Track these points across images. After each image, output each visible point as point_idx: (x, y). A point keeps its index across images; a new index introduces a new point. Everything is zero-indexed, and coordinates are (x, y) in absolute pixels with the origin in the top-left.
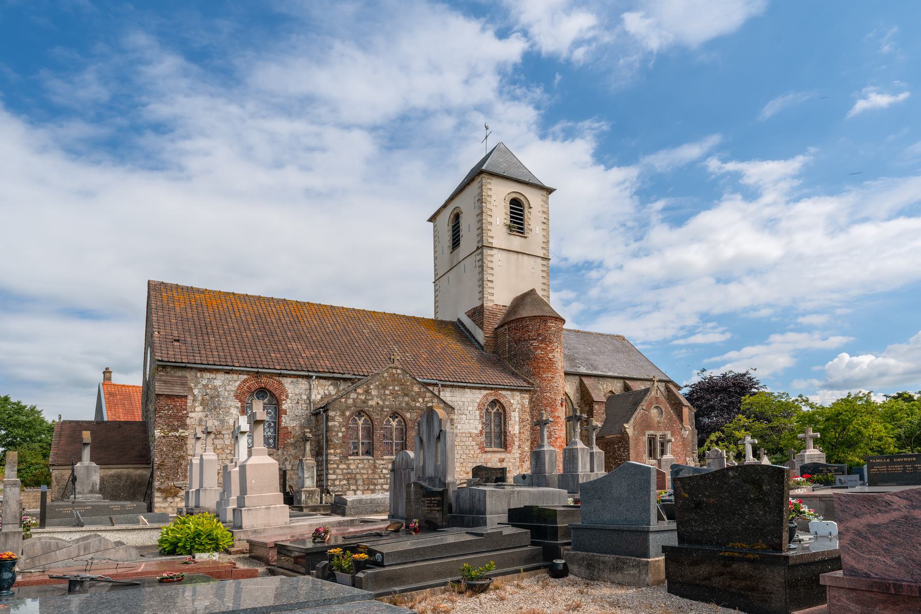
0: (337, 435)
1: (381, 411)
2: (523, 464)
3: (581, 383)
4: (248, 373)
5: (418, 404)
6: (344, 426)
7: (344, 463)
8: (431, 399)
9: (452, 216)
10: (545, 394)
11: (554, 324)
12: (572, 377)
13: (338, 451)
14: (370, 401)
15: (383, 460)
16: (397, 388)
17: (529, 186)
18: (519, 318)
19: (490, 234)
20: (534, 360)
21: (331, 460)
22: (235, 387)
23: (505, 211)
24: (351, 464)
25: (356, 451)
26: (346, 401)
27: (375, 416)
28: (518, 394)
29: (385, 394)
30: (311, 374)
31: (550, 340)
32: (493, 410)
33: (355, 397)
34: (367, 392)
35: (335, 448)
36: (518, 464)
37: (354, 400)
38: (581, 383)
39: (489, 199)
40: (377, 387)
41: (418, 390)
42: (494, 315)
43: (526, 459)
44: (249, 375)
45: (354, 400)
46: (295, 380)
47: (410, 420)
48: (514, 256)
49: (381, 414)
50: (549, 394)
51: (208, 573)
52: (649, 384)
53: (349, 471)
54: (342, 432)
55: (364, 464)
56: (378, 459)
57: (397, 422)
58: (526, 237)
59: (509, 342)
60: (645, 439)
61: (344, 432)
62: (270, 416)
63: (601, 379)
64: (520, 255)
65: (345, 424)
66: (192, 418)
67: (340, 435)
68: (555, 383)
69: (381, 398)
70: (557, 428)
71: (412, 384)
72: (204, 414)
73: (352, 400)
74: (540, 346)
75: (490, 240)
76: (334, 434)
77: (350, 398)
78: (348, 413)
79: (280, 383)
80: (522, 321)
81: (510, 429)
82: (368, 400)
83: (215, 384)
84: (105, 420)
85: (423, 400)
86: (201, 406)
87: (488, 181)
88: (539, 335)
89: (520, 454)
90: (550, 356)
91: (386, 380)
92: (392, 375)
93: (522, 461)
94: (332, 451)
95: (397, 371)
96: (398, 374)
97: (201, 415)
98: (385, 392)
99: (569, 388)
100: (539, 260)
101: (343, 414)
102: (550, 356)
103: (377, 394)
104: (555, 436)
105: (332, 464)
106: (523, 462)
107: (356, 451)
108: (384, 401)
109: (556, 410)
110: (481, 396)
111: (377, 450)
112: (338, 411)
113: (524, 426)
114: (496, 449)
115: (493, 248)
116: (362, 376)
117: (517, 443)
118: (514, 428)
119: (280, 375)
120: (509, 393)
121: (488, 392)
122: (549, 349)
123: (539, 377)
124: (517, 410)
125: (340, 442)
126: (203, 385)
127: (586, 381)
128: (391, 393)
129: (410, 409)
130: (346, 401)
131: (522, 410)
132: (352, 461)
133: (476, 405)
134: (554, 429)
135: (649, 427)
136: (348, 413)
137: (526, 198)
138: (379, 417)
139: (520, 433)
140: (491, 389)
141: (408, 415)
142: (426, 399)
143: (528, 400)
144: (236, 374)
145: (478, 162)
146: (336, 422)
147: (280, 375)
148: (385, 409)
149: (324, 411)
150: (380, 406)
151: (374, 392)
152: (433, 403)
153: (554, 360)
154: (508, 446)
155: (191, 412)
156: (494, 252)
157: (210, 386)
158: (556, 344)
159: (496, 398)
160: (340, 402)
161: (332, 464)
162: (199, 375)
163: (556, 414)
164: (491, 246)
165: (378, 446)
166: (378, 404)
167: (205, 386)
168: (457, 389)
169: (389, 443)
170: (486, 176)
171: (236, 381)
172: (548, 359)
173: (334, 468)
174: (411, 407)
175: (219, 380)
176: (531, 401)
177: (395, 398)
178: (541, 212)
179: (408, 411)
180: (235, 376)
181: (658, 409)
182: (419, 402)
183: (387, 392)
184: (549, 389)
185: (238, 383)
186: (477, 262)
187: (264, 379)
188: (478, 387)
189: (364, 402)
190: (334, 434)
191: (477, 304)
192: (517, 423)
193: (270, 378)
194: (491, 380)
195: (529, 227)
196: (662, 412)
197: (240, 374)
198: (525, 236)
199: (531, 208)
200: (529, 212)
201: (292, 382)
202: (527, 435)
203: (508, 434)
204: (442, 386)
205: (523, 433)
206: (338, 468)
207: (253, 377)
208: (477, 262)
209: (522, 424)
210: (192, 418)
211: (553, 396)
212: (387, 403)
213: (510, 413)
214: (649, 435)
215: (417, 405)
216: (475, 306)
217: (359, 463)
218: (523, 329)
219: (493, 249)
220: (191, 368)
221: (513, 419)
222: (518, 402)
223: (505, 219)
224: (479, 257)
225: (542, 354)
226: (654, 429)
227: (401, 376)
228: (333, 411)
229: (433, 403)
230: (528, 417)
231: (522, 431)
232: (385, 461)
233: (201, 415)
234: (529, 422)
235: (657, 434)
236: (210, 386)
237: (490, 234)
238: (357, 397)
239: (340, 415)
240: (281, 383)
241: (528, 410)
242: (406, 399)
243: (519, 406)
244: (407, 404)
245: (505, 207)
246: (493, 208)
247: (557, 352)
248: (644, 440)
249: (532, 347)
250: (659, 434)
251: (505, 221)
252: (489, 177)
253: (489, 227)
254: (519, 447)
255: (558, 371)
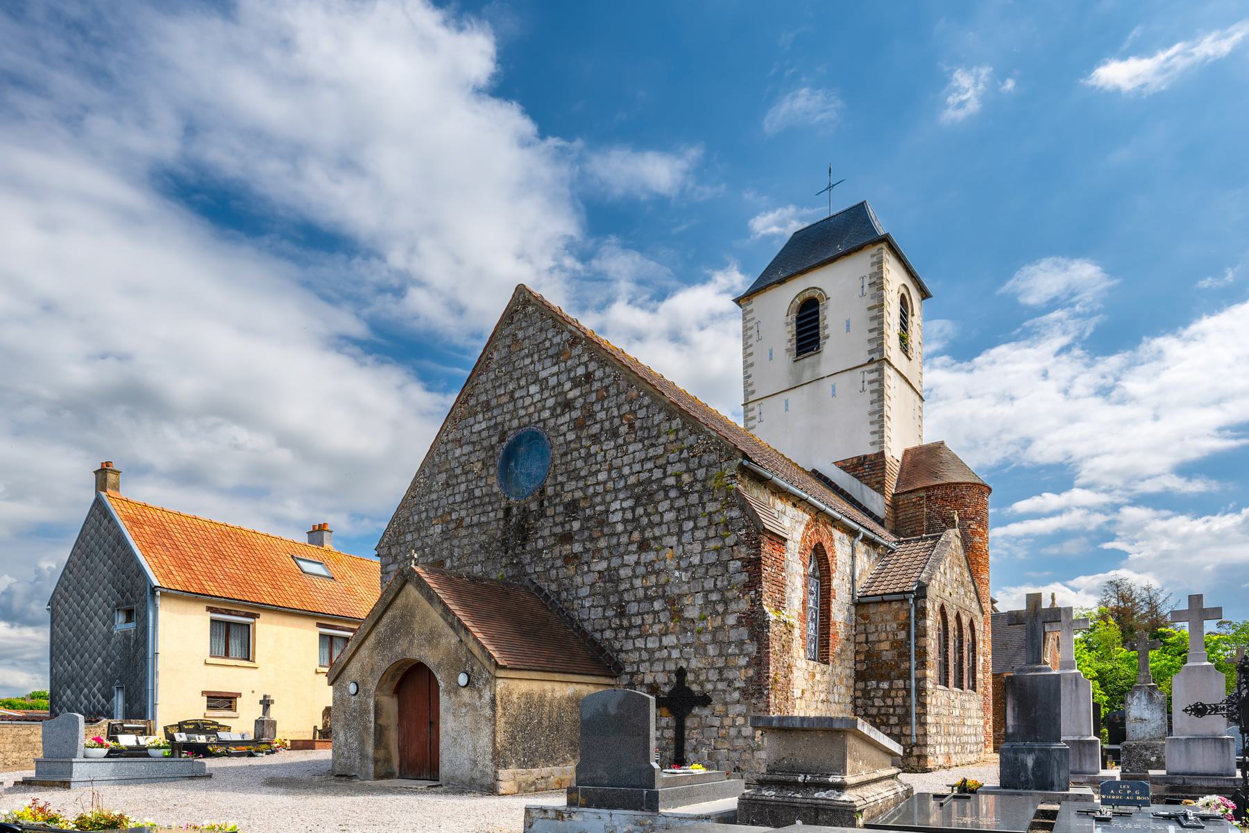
9: (798, 301)
17: (912, 280)
18: (953, 483)
20: (972, 551)
51: (254, 756)
59: (929, 519)
80: (955, 488)
84: (331, 758)
116: (834, 522)
145: (847, 207)
149: (915, 599)
186: (866, 383)
191: (871, 451)
194: (226, 590)
208: (866, 383)
216: (861, 453)
218: (956, 501)
224: (874, 376)
249: (969, 531)
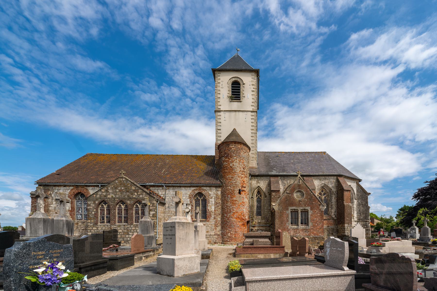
0: (92, 213)
1: (114, 200)
2: (216, 227)
3: (338, 181)
4: (73, 186)
5: (134, 196)
6: (95, 209)
7: (95, 227)
8: (141, 193)
10: (228, 188)
11: (233, 146)
12: (265, 177)
13: (92, 221)
14: (108, 196)
15: (115, 225)
16: (123, 188)
17: (242, 72)
19: (219, 104)
21: (89, 225)
22: (68, 192)
23: (228, 89)
24: (99, 227)
25: (103, 221)
26: (96, 196)
27: (110, 203)
28: (214, 188)
29: (116, 192)
30: (98, 184)
31: (231, 155)
32: (201, 198)
33: (101, 194)
34: (107, 191)
35: (91, 220)
36: (213, 228)
37: (100, 195)
38: (338, 181)
39: (218, 85)
40: (112, 188)
41: (134, 189)
42: (419, 158)
43: (219, 225)
44: (73, 187)
45: (100, 195)
46: (93, 188)
47: (129, 205)
48: (233, 114)
49: (114, 202)
50: (229, 187)
52: (323, 178)
53: (98, 231)
54: (94, 211)
55: (106, 227)
56: (113, 225)
57: (142, 206)
58: (241, 102)
60: (289, 212)
61: (95, 211)
62: (87, 205)
63: (286, 177)
64: (237, 113)
65: (95, 207)
66: (52, 207)
67: (93, 213)
68: (234, 180)
69: (114, 194)
70: (235, 207)
71: (131, 185)
72: (56, 205)
73: (99, 195)
74: (226, 160)
75: (219, 107)
76: (90, 212)
77: (98, 195)
78: (97, 202)
79: (87, 190)
81: (209, 208)
82: (108, 195)
83: (60, 192)
85: (137, 194)
86: (55, 201)
87: (218, 75)
88: (225, 153)
89: (215, 222)
90: (231, 165)
91: (117, 184)
92: (120, 182)
93: (216, 226)
94: (89, 221)
95: (122, 179)
96: (123, 181)
97: (55, 205)
98: (116, 190)
99: (262, 184)
100: (250, 113)
101: (94, 203)
102: (231, 165)
103: (112, 192)
104: (233, 212)
105: (89, 227)
106: (217, 227)
107: (103, 221)
108: (115, 195)
109: (234, 196)
110: (190, 191)
111: (112, 220)
112: (92, 201)
113: (218, 206)
114: (203, 219)
115: (220, 111)
117: (213, 216)
118: (211, 207)
119: (87, 186)
120: (208, 188)
121: (195, 188)
122: (230, 161)
123: (225, 178)
124: (213, 197)
125: (93, 216)
126: (56, 192)
127: (341, 179)
128: (120, 191)
129: (130, 199)
130: (96, 196)
131: (217, 198)
132: (99, 226)
133: (188, 196)
134: (233, 208)
135: (292, 204)
136: (97, 202)
137: (241, 79)
138: (113, 204)
139: (215, 210)
140: (197, 186)
141: (129, 202)
142: (139, 193)
143: (220, 192)
144: (68, 187)
146: (91, 206)
147: (87, 186)
148: (116, 200)
150: (113, 198)
151: (110, 191)
152: (143, 195)
153: (233, 167)
154: (207, 218)
155: (51, 204)
156: (222, 113)
157: (58, 193)
158: (235, 158)
159: (200, 191)
160: (93, 196)
161: (89, 227)
162: (54, 188)
163: (235, 199)
164: (220, 110)
165: (113, 218)
166: (112, 197)
167: (56, 193)
168: (177, 188)
169: (121, 216)
170: (217, 73)
171: (68, 190)
172: (229, 167)
173: (90, 229)
174: (130, 198)
175: (62, 190)
176: (222, 193)
177: (122, 193)
178: (251, 85)
179: (128, 200)
180: (68, 188)
181: (301, 193)
182: (135, 195)
183: (117, 191)
184: (230, 184)
185: (69, 191)
187: (80, 188)
188: (188, 186)
189: (105, 196)
190: (90, 212)
192: (213, 205)
193: (82, 187)
195: (243, 95)
196: (304, 194)
197: (70, 187)
198: (241, 101)
199: (244, 84)
200: (243, 87)
201: (92, 189)
202: (219, 211)
203: (207, 211)
204: (101, 186)
205: (217, 210)
206: (92, 229)
207: (75, 188)
209: (216, 205)
210: (52, 207)
211: (232, 188)
212: (117, 196)
213: (209, 200)
214: (291, 210)
215: (134, 196)
217: (103, 227)
219: (221, 112)
220: (51, 185)
221: (211, 203)
222: (214, 193)
223: (228, 94)
225: (226, 164)
226: (295, 205)
227: (125, 182)
228: (90, 201)
229: (143, 195)
230: (220, 201)
231: (216, 209)
232: (116, 226)
233: (55, 205)
234: (220, 204)
235: (298, 209)
236: (58, 193)
237: (219, 104)
238: (102, 194)
239: (93, 203)
240: (88, 190)
241: (220, 197)
242: (128, 193)
243: (215, 195)
244: (128, 196)
245: (228, 87)
246: (221, 89)
247: (236, 162)
248: (287, 213)
250: (300, 209)
251: (228, 95)
252: (219, 72)
253: (219, 100)
254: (215, 218)
255: (236, 173)
